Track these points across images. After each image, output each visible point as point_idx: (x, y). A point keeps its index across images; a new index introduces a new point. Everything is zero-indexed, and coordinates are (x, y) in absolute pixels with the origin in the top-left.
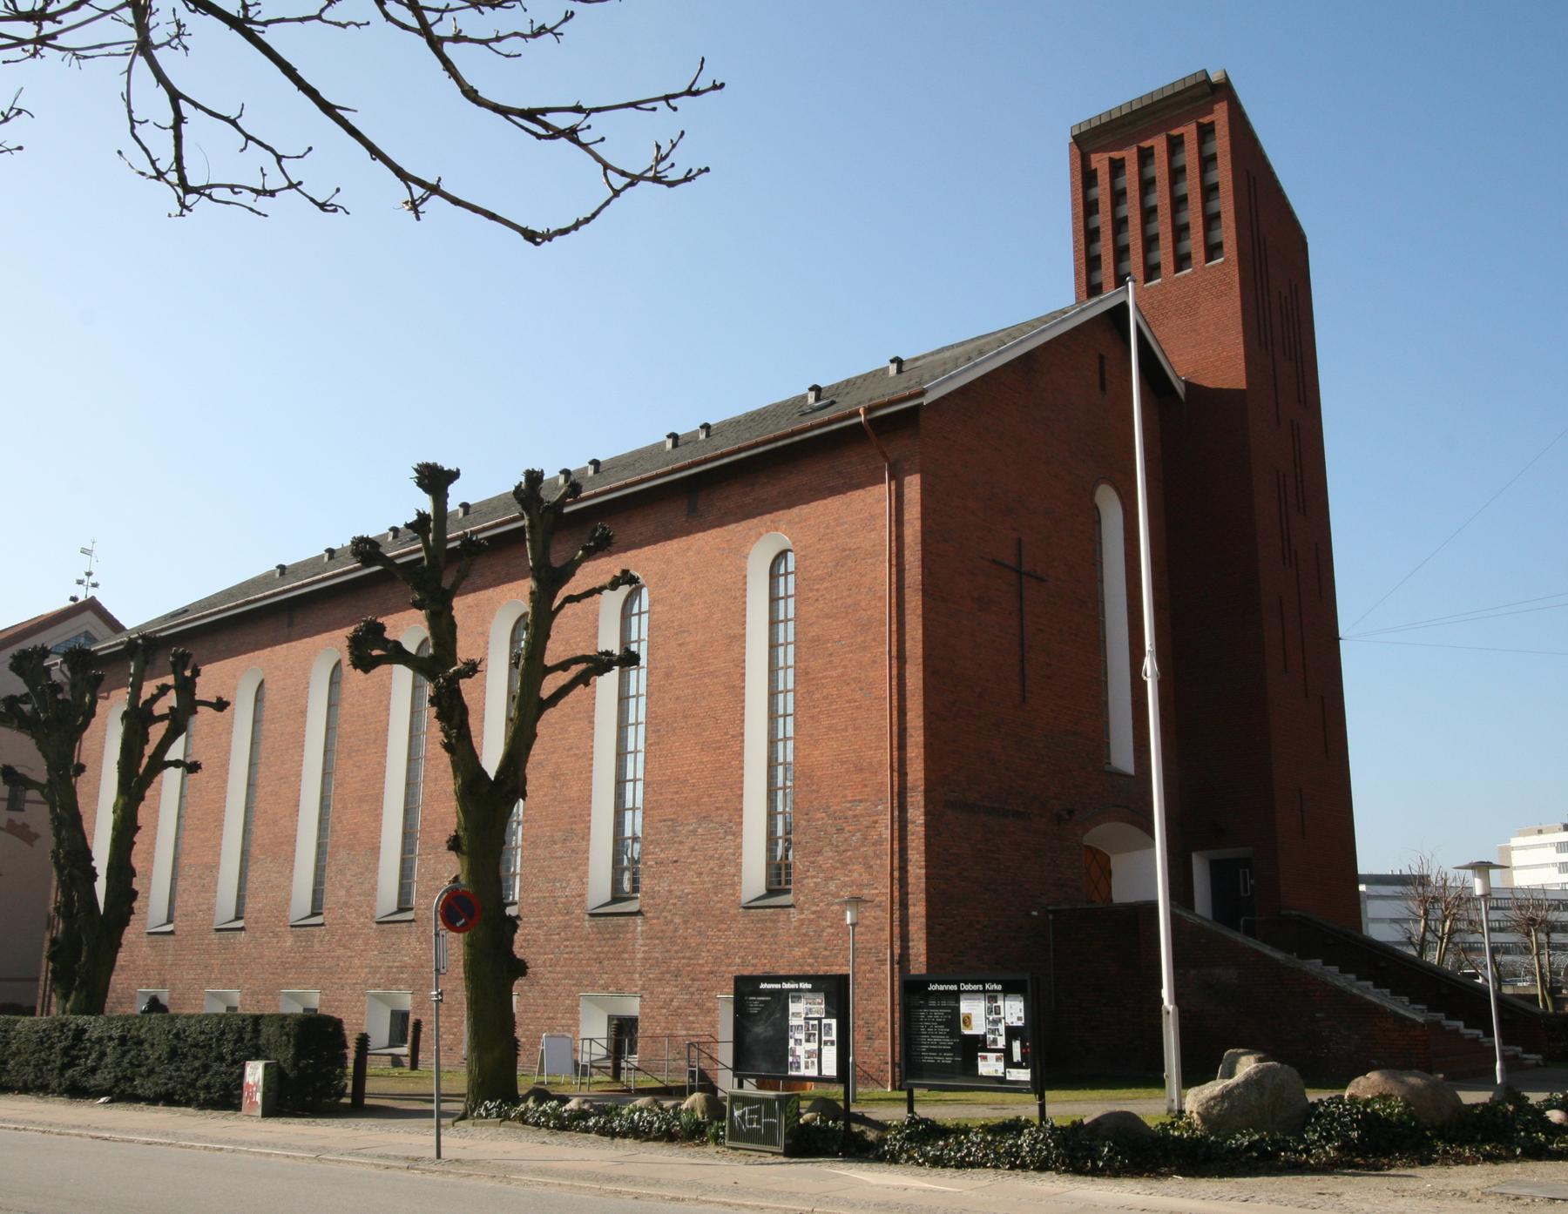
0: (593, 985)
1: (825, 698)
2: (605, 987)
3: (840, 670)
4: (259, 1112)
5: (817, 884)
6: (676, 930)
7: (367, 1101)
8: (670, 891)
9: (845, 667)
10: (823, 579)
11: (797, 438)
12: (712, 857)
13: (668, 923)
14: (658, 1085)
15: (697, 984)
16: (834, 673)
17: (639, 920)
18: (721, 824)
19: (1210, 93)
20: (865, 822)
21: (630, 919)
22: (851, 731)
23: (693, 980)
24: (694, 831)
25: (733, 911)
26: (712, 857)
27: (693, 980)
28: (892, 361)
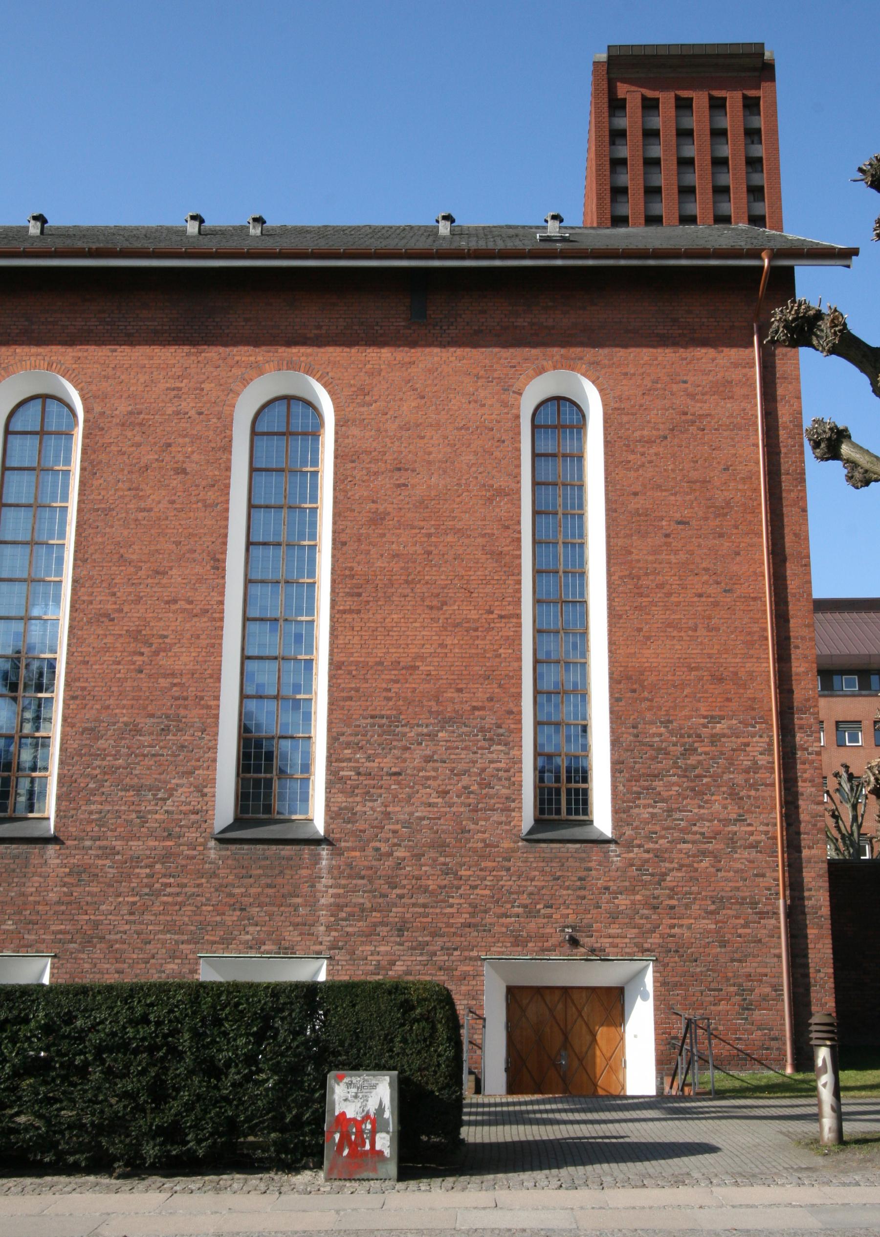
0: (226, 942)
1: (661, 586)
2: (256, 945)
3: (682, 556)
4: (392, 1169)
5: (653, 815)
6: (399, 866)
7: (470, 1134)
8: (387, 815)
9: (691, 553)
10: (650, 442)
11: (651, 262)
12: (465, 772)
13: (381, 856)
14: (737, 1084)
15: (439, 942)
16: (673, 558)
17: (324, 851)
18: (482, 730)
19: (609, 47)
20: (730, 743)
21: (36, 849)
22: (702, 632)
23: (434, 935)
24: (432, 736)
25: (506, 844)
26: (465, 772)
27: (434, 935)
28: (35, 218)
